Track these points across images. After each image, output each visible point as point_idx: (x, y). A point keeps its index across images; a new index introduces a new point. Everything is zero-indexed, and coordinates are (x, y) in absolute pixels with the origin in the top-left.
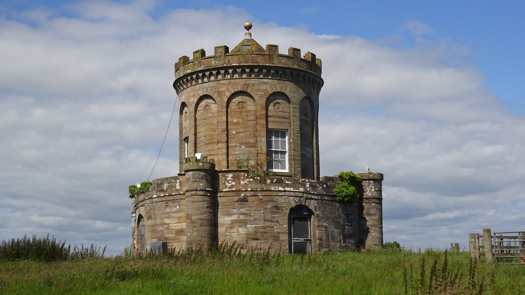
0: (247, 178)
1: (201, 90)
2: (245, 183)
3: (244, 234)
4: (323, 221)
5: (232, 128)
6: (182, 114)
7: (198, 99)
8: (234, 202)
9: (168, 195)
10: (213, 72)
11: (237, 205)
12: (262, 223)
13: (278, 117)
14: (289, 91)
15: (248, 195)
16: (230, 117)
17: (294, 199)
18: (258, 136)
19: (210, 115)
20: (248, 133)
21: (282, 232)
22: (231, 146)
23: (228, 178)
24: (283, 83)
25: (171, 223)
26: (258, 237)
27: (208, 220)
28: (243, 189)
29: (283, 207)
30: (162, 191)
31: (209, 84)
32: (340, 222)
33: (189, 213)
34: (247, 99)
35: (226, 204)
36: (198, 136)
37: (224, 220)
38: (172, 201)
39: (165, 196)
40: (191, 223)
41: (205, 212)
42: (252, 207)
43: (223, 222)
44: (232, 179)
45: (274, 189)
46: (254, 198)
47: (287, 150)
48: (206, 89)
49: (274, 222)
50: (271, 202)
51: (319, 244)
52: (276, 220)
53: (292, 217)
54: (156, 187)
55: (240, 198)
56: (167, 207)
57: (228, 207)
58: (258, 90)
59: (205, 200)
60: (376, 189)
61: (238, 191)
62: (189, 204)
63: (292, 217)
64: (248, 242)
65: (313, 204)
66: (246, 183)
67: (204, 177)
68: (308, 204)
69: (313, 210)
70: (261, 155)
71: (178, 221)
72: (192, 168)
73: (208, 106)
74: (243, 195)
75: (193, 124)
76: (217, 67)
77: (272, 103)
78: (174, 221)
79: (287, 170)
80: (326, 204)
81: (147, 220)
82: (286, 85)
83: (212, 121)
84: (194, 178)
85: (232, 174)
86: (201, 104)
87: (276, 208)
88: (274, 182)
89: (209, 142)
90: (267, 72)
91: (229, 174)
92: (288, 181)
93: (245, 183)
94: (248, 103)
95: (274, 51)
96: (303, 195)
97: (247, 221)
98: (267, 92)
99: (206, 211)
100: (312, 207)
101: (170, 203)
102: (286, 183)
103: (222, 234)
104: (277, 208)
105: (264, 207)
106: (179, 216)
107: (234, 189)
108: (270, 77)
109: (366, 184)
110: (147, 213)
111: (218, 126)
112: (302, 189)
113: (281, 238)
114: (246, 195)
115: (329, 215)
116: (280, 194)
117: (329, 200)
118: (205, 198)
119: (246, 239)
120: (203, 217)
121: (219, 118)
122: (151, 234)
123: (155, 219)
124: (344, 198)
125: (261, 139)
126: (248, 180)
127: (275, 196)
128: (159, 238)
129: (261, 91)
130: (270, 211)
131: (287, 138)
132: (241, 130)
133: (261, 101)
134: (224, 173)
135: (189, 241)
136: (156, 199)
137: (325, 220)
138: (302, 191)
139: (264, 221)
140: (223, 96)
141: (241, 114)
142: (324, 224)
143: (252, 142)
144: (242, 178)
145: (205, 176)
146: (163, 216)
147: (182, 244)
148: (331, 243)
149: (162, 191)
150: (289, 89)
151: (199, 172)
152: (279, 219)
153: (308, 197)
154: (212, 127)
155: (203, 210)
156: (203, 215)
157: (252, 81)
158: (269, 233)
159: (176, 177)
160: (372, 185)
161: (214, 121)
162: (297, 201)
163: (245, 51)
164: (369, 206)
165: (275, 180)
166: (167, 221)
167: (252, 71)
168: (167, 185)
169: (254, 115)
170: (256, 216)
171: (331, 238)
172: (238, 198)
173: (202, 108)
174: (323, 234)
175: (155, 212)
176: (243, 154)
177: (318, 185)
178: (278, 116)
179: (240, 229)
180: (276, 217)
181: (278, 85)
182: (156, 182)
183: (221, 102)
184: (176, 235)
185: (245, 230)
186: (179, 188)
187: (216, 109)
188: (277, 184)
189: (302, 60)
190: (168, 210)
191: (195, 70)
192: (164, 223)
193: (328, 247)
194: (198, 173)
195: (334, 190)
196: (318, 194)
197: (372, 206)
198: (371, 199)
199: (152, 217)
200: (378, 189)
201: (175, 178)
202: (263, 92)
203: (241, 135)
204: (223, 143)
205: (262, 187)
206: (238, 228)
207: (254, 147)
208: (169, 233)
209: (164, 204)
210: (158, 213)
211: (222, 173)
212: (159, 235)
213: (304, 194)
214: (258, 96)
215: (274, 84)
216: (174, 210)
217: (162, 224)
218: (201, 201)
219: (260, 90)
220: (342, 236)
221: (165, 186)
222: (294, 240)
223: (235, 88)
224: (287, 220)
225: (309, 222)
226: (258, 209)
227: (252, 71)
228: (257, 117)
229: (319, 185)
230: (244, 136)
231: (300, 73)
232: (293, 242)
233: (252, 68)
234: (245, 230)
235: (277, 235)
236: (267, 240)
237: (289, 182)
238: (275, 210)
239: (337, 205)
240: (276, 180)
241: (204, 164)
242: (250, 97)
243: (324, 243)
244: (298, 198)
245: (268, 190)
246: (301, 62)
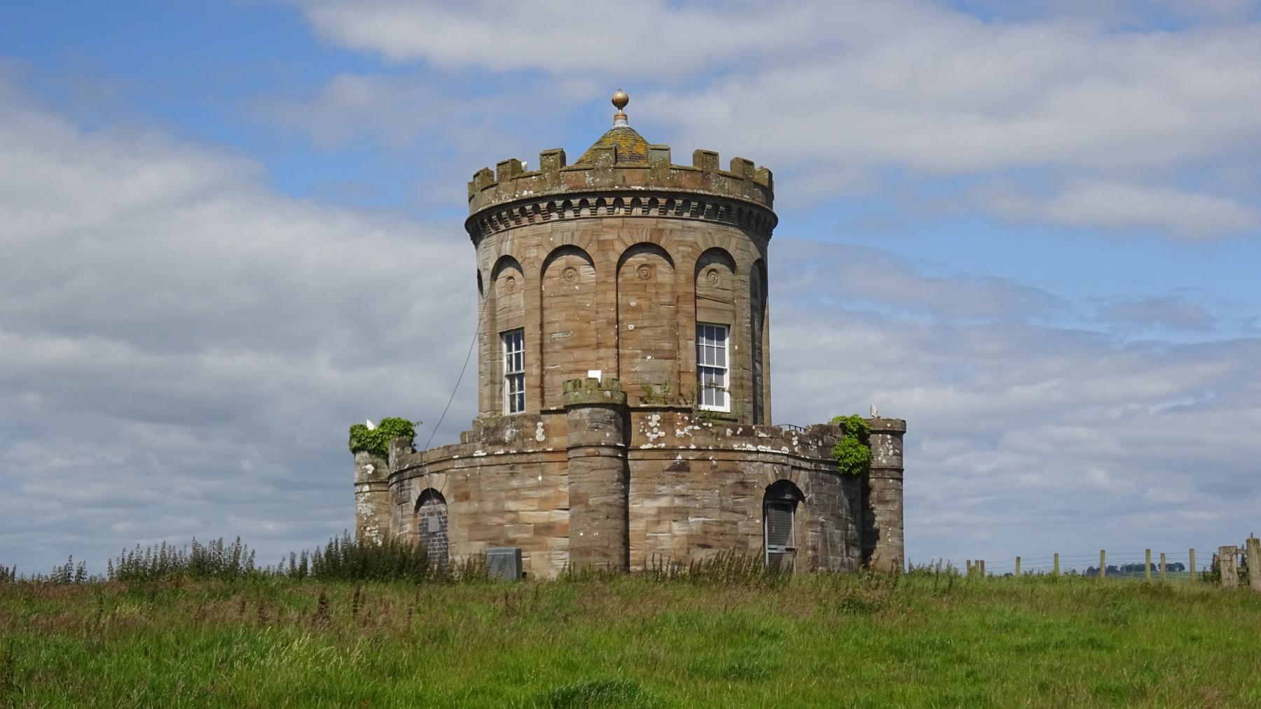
0: (689, 423)
1: (558, 236)
2: (685, 434)
3: (683, 535)
4: (818, 513)
5: (626, 319)
6: (495, 279)
7: (550, 254)
8: (663, 471)
9: (515, 452)
10: (588, 199)
11: (669, 476)
15: (690, 458)
16: (622, 295)
17: (773, 469)
18: (680, 337)
19: (577, 287)
20: (659, 330)
21: (753, 533)
22: (625, 355)
23: (650, 423)
25: (522, 511)
26: (709, 542)
27: (620, 507)
28: (681, 446)
29: (754, 483)
30: (501, 443)
31: (577, 224)
32: (842, 515)
33: (582, 492)
34: (658, 260)
35: (647, 475)
36: (547, 329)
37: (641, 507)
38: (525, 465)
39: (507, 454)
40: (586, 512)
42: (698, 482)
43: (641, 511)
44: (658, 425)
45: (738, 447)
46: (701, 464)
47: (727, 366)
48: (569, 234)
54: (482, 433)
55: (674, 463)
56: (513, 476)
57: (650, 480)
58: (681, 243)
61: (671, 451)
62: (580, 474)
64: (691, 552)
65: (803, 478)
66: (687, 433)
67: (613, 420)
70: (687, 376)
71: (539, 506)
72: (590, 402)
73: (572, 268)
74: (680, 457)
75: (538, 304)
76: (598, 190)
77: (704, 269)
78: (530, 506)
79: (726, 408)
80: (823, 479)
81: (455, 502)
82: (731, 234)
83: (582, 301)
84: (592, 420)
85: (660, 415)
86: (554, 262)
88: (738, 433)
89: (576, 343)
91: (654, 415)
93: (685, 434)
94: (660, 268)
97: (689, 510)
98: (697, 248)
99: (616, 488)
100: (801, 486)
101: (519, 469)
102: (760, 436)
103: (640, 535)
104: (744, 486)
105: (720, 483)
106: (543, 496)
107: (663, 445)
109: (877, 441)
110: (456, 488)
111: (597, 312)
112: (785, 450)
113: (750, 544)
114: (687, 458)
115: (826, 501)
116: (749, 458)
119: (686, 546)
120: (610, 499)
121: (600, 297)
122: (469, 530)
123: (481, 501)
124: (852, 468)
125: (687, 344)
126: (691, 427)
127: (740, 461)
128: (490, 539)
129: (686, 245)
131: (727, 341)
132: (646, 323)
133: (687, 264)
134: (642, 413)
135: (581, 547)
136: (483, 459)
138: (787, 453)
139: (720, 510)
140: (609, 250)
141: (645, 290)
142: (820, 519)
143: (667, 349)
144: (678, 424)
145: (614, 417)
146: (503, 495)
147: (550, 554)
149: (501, 443)
150: (734, 241)
151: (603, 410)
152: (748, 508)
153: (795, 465)
154: (582, 312)
155: (612, 487)
156: (611, 497)
158: (729, 534)
159: (535, 415)
160: (889, 444)
161: (587, 301)
162: (777, 472)
163: (658, 160)
164: (883, 484)
165: (741, 429)
166: (511, 505)
167: (670, 204)
168: (512, 432)
169: (670, 292)
171: (831, 546)
172: (672, 464)
173: (556, 273)
175: (479, 487)
176: (650, 372)
177: (810, 442)
178: (714, 296)
179: (675, 526)
180: (742, 504)
181: (716, 234)
182: (485, 424)
183: (604, 263)
184: (534, 534)
185: (684, 528)
186: (544, 438)
187: (594, 276)
188: (745, 438)
189: (724, 175)
190: (516, 484)
191: (546, 193)
192: (505, 509)
193: (826, 565)
194: (602, 412)
195: (833, 452)
198: (886, 472)
199: (472, 495)
201: (533, 419)
202: (691, 246)
203: (644, 332)
204: (609, 347)
205: (717, 444)
206: (670, 524)
207: (672, 359)
208: (519, 530)
209: (504, 471)
210: (489, 489)
211: (638, 413)
212: (492, 534)
213: (790, 459)
214: (679, 255)
215: (710, 231)
216: (530, 484)
217: (500, 512)
221: (508, 435)
222: (769, 549)
223: (636, 236)
225: (793, 514)
226: (710, 487)
227: (670, 204)
228: (678, 297)
230: (652, 336)
233: (671, 197)
234: (684, 528)
238: (740, 490)
241: (614, 394)
242: (663, 257)
243: (820, 556)
245: (727, 450)
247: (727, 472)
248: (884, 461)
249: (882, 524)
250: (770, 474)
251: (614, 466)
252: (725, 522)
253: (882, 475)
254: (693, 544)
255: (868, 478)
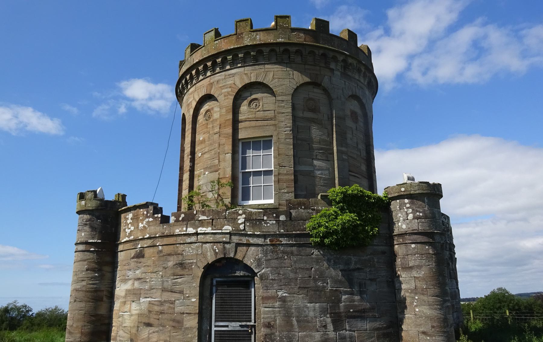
2: (144, 226)
12: (159, 294)
13: (254, 120)
14: (271, 77)
17: (213, 248)
21: (188, 312)
24: (261, 69)
26: (152, 321)
27: (87, 292)
29: (192, 263)
34: (214, 104)
41: (82, 279)
45: (180, 231)
46: (151, 250)
49: (176, 292)
50: (173, 255)
51: (266, 335)
52: (180, 288)
53: (215, 282)
59: (85, 258)
60: (418, 213)
63: (215, 282)
68: (242, 256)
69: (252, 267)
87: (180, 267)
88: (180, 219)
90: (233, 59)
92: (204, 215)
95: (243, 28)
96: (230, 238)
100: (250, 261)
102: (199, 219)
104: (182, 267)
105: (163, 265)
108: (239, 65)
112: (228, 228)
113: (185, 323)
115: (292, 275)
116: (189, 240)
117: (292, 245)
118: (86, 255)
126: (147, 220)
127: (181, 244)
129: (227, 88)
130: (172, 272)
133: (227, 100)
137: (281, 286)
141: (207, 128)
148: (297, 334)
152: (185, 287)
157: (217, 77)
158: (167, 313)
160: (408, 208)
164: (404, 249)
165: (183, 215)
170: (153, 282)
174: (274, 313)
177: (265, 218)
180: (180, 284)
188: (185, 223)
196: (265, 235)
197: (410, 250)
200: (421, 214)
205: (163, 231)
213: (233, 237)
215: (246, 72)
218: (80, 261)
219: (227, 86)
220: (328, 316)
222: (216, 326)
224: (198, 289)
229: (268, 218)
231: (290, 49)
232: (215, 331)
235: (178, 318)
236: (164, 326)
237: (205, 218)
238: (179, 271)
239: (316, 252)
240: (184, 216)
243: (277, 333)
244: (220, 246)
246: (292, 32)
247: (169, 255)
248: (404, 226)
249: (408, 292)
250: (209, 254)
251: (86, 258)
252: (165, 301)
253: (403, 241)
254: (141, 322)
255: (394, 245)
